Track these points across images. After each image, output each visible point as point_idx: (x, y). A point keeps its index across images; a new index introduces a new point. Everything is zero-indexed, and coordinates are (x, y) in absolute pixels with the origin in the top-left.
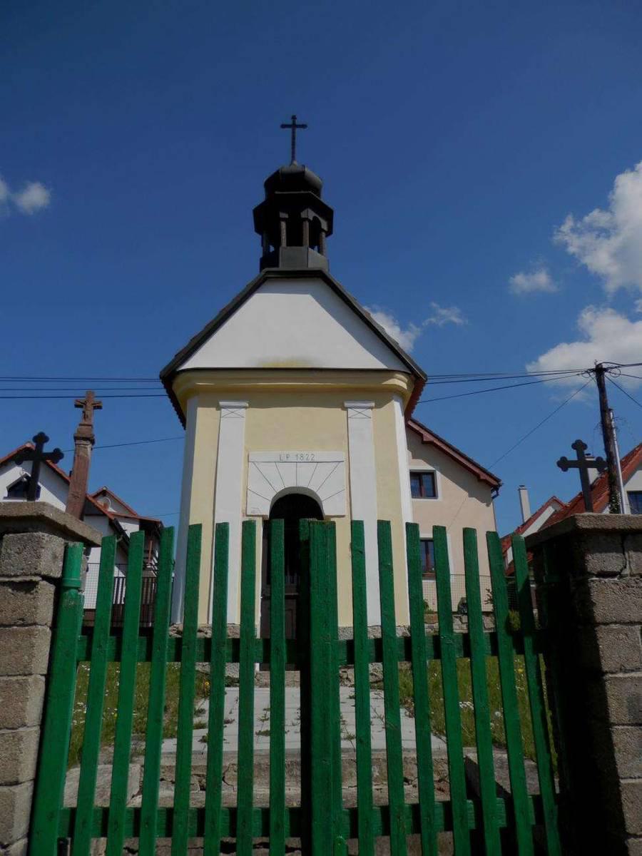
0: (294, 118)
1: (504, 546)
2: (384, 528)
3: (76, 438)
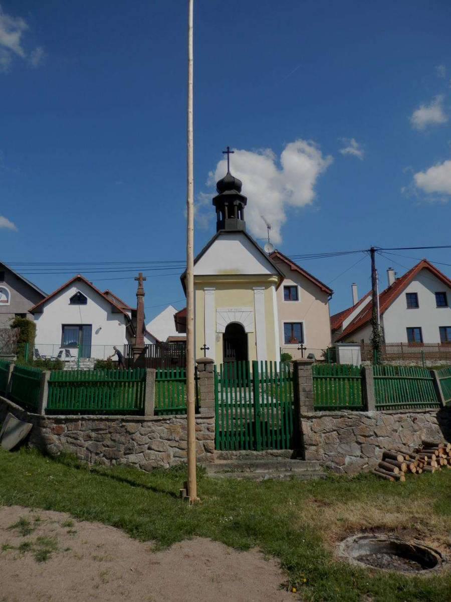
1: (341, 319)
2: (266, 362)
3: (137, 295)
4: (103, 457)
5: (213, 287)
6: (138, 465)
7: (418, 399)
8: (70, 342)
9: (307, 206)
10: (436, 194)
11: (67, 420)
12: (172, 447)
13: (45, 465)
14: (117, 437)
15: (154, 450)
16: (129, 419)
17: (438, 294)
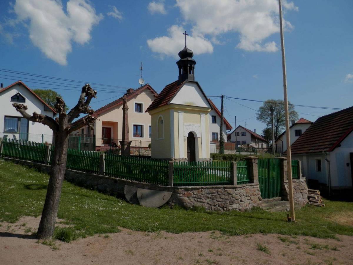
4: (218, 207)
5: (182, 111)
6: (238, 210)
8: (9, 129)
9: (86, 44)
10: (157, 54)
11: (192, 189)
12: (248, 199)
13: (182, 213)
14: (223, 196)
15: (243, 201)
16: (229, 187)
17: (213, 116)
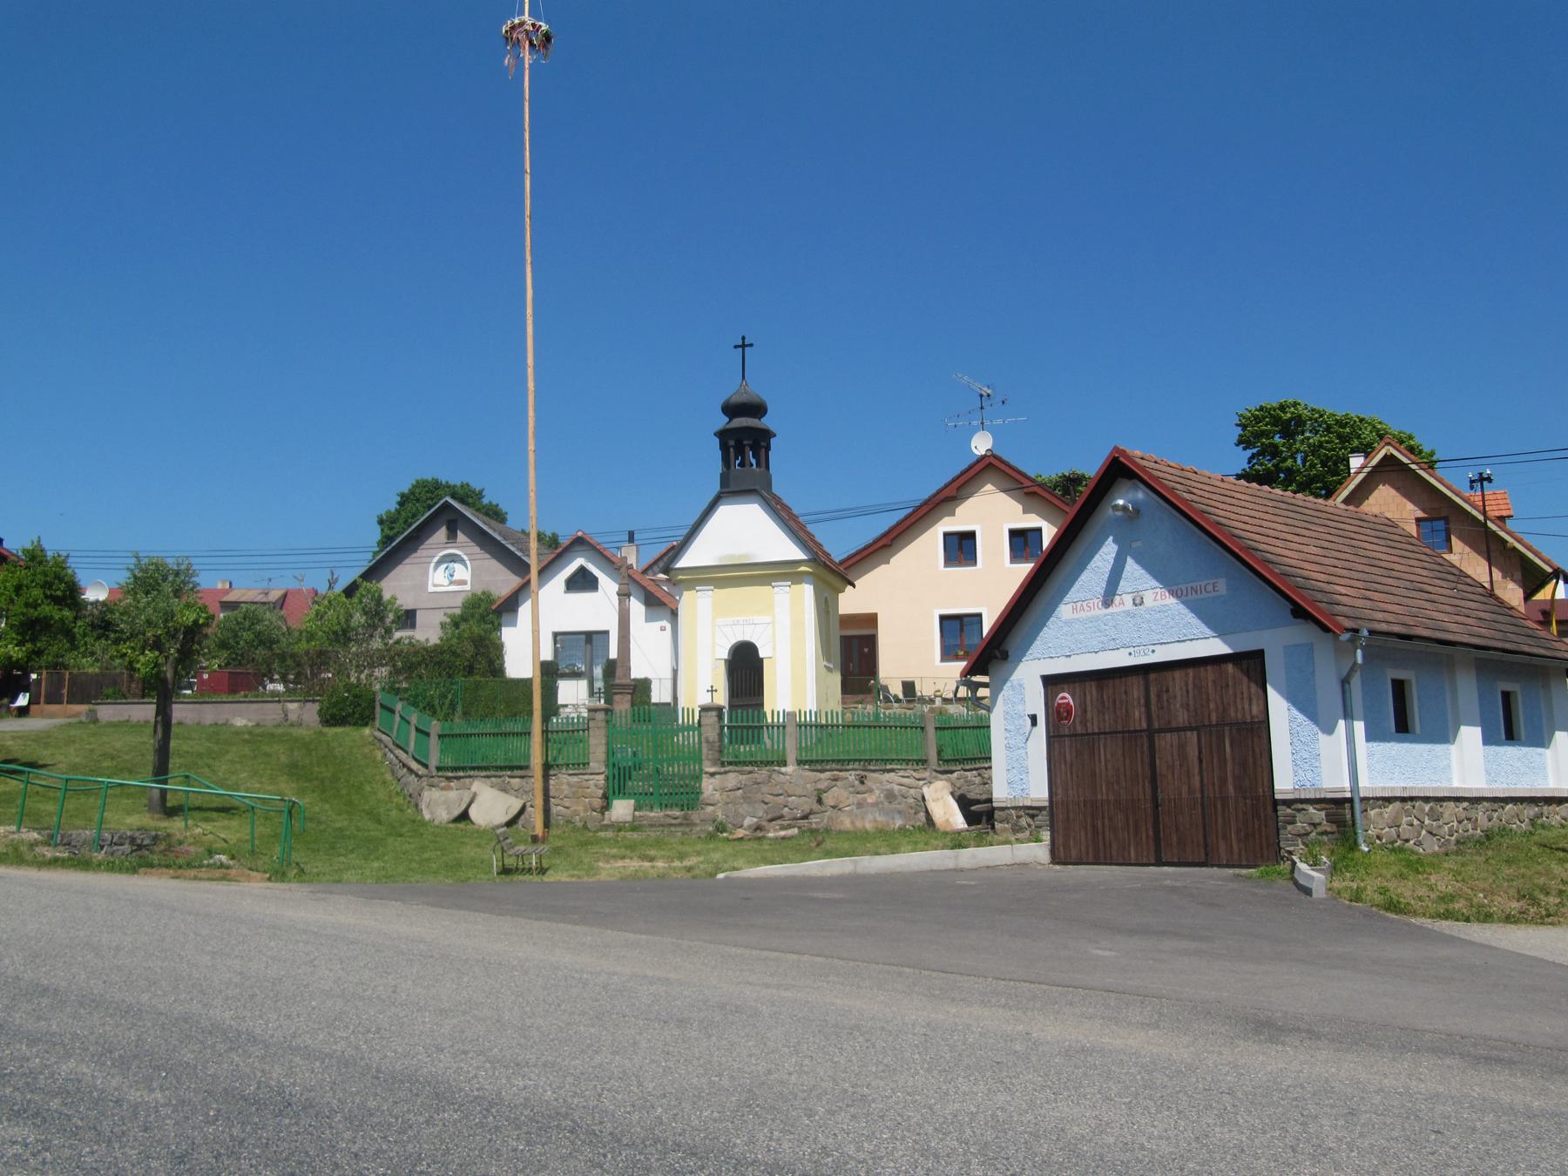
0: (743, 338)
7: (742, 739)
